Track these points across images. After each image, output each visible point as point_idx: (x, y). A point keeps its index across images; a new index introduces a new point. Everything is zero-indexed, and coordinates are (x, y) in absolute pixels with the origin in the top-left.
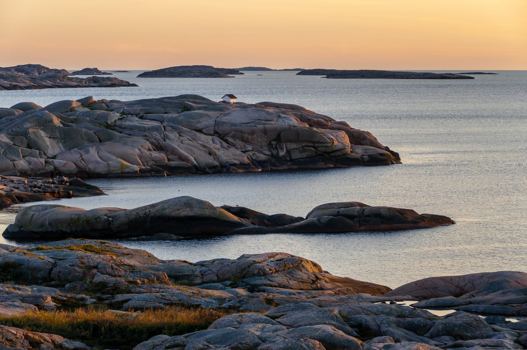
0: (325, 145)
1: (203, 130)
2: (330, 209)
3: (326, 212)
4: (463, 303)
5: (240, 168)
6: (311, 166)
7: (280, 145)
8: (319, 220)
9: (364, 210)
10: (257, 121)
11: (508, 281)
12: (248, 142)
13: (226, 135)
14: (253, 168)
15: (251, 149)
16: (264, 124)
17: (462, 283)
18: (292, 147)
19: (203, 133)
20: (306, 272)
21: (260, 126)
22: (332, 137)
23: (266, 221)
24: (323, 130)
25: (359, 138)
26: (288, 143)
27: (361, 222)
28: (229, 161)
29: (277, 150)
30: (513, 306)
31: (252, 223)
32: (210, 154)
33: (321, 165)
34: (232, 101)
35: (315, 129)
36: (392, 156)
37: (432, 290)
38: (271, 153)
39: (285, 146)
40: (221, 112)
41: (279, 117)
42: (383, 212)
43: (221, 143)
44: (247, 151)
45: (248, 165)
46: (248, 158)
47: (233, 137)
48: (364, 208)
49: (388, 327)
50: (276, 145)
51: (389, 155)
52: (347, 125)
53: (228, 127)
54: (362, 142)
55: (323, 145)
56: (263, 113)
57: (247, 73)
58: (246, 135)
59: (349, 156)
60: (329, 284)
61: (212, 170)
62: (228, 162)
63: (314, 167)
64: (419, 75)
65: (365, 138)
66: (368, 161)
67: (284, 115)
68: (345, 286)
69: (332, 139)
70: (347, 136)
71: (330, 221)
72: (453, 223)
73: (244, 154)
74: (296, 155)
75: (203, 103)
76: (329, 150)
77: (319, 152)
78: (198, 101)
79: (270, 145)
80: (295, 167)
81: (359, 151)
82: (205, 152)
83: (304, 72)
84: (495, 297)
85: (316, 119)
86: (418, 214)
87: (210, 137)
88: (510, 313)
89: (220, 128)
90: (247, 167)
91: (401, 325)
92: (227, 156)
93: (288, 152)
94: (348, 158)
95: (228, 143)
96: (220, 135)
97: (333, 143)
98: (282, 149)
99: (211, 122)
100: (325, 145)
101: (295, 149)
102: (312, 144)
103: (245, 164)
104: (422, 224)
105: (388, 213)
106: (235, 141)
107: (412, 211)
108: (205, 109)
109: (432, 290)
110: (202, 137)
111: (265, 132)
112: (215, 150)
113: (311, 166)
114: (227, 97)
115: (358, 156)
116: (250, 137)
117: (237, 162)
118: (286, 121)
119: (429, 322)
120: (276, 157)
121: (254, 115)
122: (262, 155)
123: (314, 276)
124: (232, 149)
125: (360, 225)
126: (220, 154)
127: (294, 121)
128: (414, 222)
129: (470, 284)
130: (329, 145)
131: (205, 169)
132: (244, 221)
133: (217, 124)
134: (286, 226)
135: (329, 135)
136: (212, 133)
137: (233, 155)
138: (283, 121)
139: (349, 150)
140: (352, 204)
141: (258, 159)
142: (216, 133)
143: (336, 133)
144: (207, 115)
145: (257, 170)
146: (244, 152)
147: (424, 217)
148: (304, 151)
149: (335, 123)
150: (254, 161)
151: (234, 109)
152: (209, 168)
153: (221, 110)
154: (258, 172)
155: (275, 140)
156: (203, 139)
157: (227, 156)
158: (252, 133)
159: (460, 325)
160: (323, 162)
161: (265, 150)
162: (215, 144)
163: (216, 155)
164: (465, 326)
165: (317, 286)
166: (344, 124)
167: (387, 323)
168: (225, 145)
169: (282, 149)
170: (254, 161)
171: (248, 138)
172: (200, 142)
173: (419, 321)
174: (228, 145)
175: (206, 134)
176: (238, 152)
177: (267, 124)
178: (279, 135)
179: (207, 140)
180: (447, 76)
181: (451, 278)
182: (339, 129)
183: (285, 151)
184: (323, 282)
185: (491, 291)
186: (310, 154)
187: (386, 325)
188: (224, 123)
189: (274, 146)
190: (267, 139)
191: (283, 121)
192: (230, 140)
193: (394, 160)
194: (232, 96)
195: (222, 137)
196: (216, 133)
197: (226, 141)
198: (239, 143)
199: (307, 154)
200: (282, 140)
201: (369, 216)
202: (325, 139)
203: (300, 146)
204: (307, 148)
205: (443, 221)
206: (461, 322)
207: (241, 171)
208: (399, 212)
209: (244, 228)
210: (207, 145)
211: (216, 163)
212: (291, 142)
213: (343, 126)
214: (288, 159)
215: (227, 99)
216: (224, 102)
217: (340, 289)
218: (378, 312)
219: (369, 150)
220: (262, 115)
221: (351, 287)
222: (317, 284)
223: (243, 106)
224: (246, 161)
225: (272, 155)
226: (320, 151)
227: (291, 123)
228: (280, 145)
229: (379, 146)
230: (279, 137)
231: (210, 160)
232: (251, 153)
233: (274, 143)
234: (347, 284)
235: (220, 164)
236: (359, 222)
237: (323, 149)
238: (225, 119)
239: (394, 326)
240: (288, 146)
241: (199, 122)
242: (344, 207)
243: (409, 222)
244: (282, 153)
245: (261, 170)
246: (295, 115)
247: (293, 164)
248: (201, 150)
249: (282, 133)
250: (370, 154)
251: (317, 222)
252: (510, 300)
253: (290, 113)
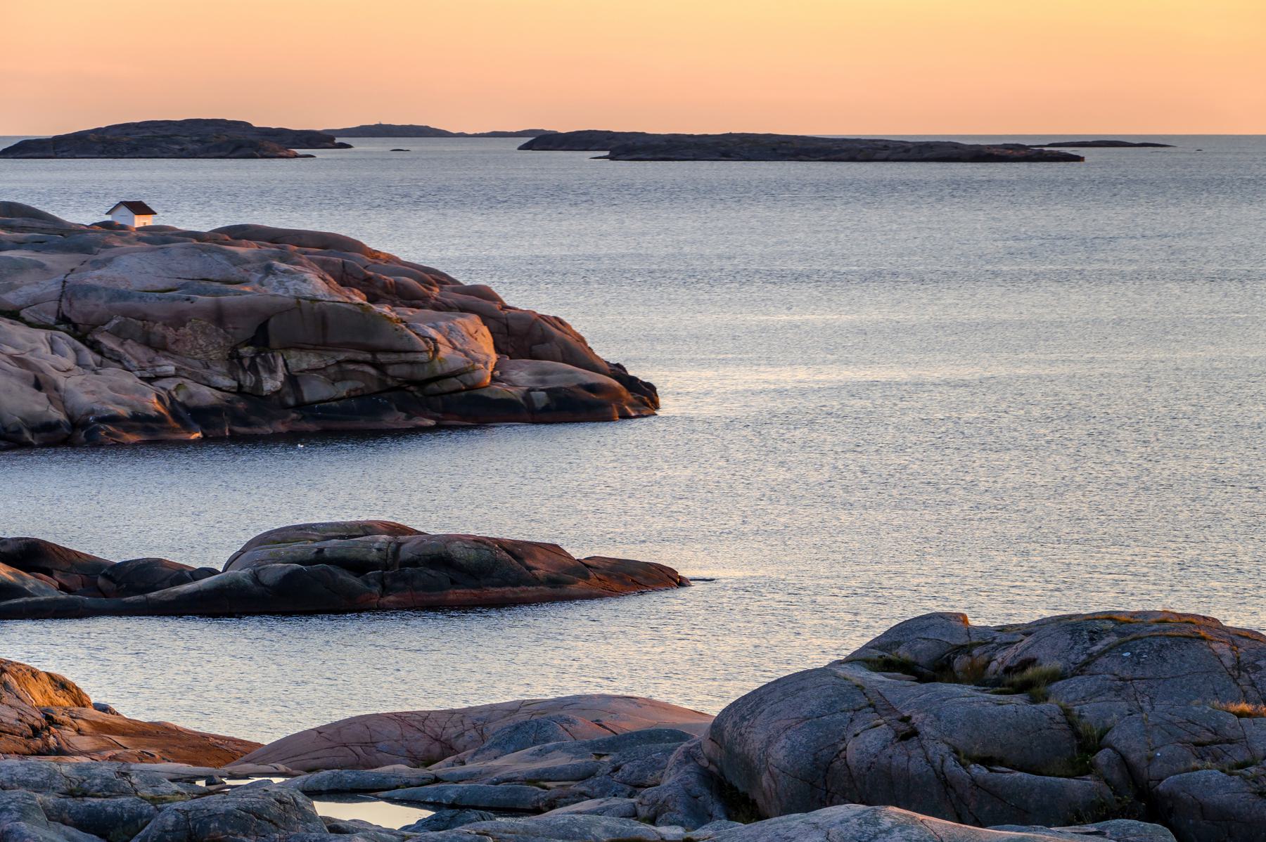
0: (411, 357)
1: (23, 313)
2: (297, 541)
3: (283, 550)
4: (414, 781)
5: (129, 430)
6: (362, 423)
7: (265, 360)
8: (256, 577)
9: (399, 545)
10: (196, 285)
11: (567, 720)
12: (165, 349)
13: (94, 326)
14: (174, 431)
15: (171, 369)
16: (217, 293)
17: (451, 730)
18: (305, 366)
19: (22, 320)
20: (15, 702)
21: (204, 300)
22: (432, 333)
23: (101, 581)
24: (408, 312)
25: (524, 336)
26: (292, 353)
27: (388, 581)
28: (97, 407)
29: (257, 373)
30: (544, 787)
31: (62, 587)
32: (38, 386)
33: (395, 419)
34: (140, 221)
35: (385, 310)
36: (624, 392)
37: (359, 750)
38: (235, 384)
39: (280, 362)
40: (83, 257)
41: (269, 270)
42: (458, 551)
43: (76, 351)
44: (158, 378)
45: (160, 419)
46: (159, 398)
47: (117, 333)
48: (401, 538)
49: (18, 820)
50: (253, 359)
51: (615, 388)
52: (492, 297)
53: (101, 302)
54: (537, 349)
55: (403, 357)
56: (217, 257)
57: (361, 146)
58: (158, 328)
59: (485, 393)
60: (87, 739)
61: (44, 434)
62: (92, 412)
63: (372, 425)
64: (907, 150)
65: (546, 338)
66: (546, 409)
67: (284, 266)
68: (137, 746)
69: (435, 341)
70: (485, 330)
71: (290, 577)
72: (682, 583)
73: (147, 387)
74: (316, 390)
75: (32, 229)
76: (423, 373)
77: (390, 382)
78: (18, 221)
79: (234, 360)
80: (311, 426)
81: (523, 376)
82: (24, 378)
83: (543, 141)
84: (516, 763)
85: (392, 279)
86: (569, 557)
87: (42, 334)
88: (529, 807)
89: (77, 304)
90: (154, 425)
91: (65, 815)
92: (93, 393)
93: (293, 380)
94: (487, 399)
95: (101, 353)
96: (75, 326)
97: (436, 351)
98: (272, 371)
99: (51, 287)
100: (411, 357)
101: (315, 370)
102: (369, 356)
103: (149, 418)
104: (580, 586)
105: (473, 553)
106: (122, 344)
107: (555, 549)
108: (38, 246)
109: (359, 750)
110: (19, 332)
111: (219, 316)
112: (55, 375)
113: (362, 423)
114: (124, 211)
115: (515, 393)
116: (170, 334)
117: (123, 411)
118: (290, 284)
119: (148, 807)
120: (253, 396)
121: (186, 265)
122: (206, 390)
123: (39, 716)
124: (113, 373)
125: (386, 590)
126: (71, 386)
127: (314, 284)
128: (553, 582)
129: (473, 732)
130: (423, 357)
131: (19, 431)
132: (30, 581)
133: (67, 292)
134: (152, 595)
135: (424, 327)
136: (52, 319)
137: (112, 389)
138: (281, 283)
139: (486, 375)
140: (367, 529)
141: (194, 402)
142: (63, 319)
143: (447, 319)
144: (41, 266)
145: (184, 436)
146: (149, 380)
147: (585, 568)
148: (343, 376)
149: (454, 290)
150: (181, 410)
151: (127, 246)
152: (34, 430)
153: (84, 249)
154: (189, 442)
155: (248, 343)
156: (20, 340)
157: (93, 393)
158: (178, 320)
159: (228, 813)
160: (400, 409)
161: (219, 374)
162: (56, 356)
163: (57, 389)
164: (241, 818)
165: (47, 744)
166: (483, 293)
167: (21, 810)
168: (90, 357)
169: (272, 371)
170: (181, 410)
171: (164, 337)
172: (10, 350)
173: (121, 806)
174: (98, 358)
175: (30, 325)
176: (130, 380)
177: (226, 293)
178: (263, 328)
179: (34, 343)
180: (995, 152)
181: (425, 717)
182: (464, 309)
183: (281, 375)
184: (68, 733)
185: (512, 748)
186: (361, 385)
187: (16, 815)
188: (90, 290)
189: (247, 362)
190: (225, 338)
191: (281, 283)
192: (108, 342)
193: (631, 405)
194: (140, 208)
195: (82, 332)
196: (63, 319)
197: (95, 346)
198: (135, 352)
199: (350, 385)
200: (274, 343)
201: (412, 563)
202: (410, 339)
203: (331, 362)
204: (351, 367)
205: (661, 578)
206: (231, 806)
207: (132, 438)
208: (508, 552)
209: (21, 600)
210: (32, 359)
211: (57, 415)
212: (301, 349)
213: (479, 301)
214: (291, 401)
215: (123, 217)
216: (106, 225)
217: (117, 752)
218: (12, 781)
219: (552, 373)
220: (216, 265)
221: (156, 746)
222: (45, 740)
223: (161, 237)
224: (152, 404)
225: (240, 390)
226: (393, 378)
227: (307, 290)
228: (265, 360)
229: (592, 364)
230: (262, 334)
231: (39, 405)
232: (170, 385)
233: (246, 351)
234: (146, 740)
235: (70, 417)
236: (381, 580)
237: (404, 370)
238: (93, 277)
239: (42, 817)
240: (292, 362)
241: (11, 287)
242: (342, 537)
243: (536, 581)
244: (271, 384)
245: (199, 435)
246: (324, 265)
247: (304, 418)
248: (11, 374)
249: (272, 320)
250: (555, 386)
251: (249, 582)
252: (546, 771)
253: (304, 259)
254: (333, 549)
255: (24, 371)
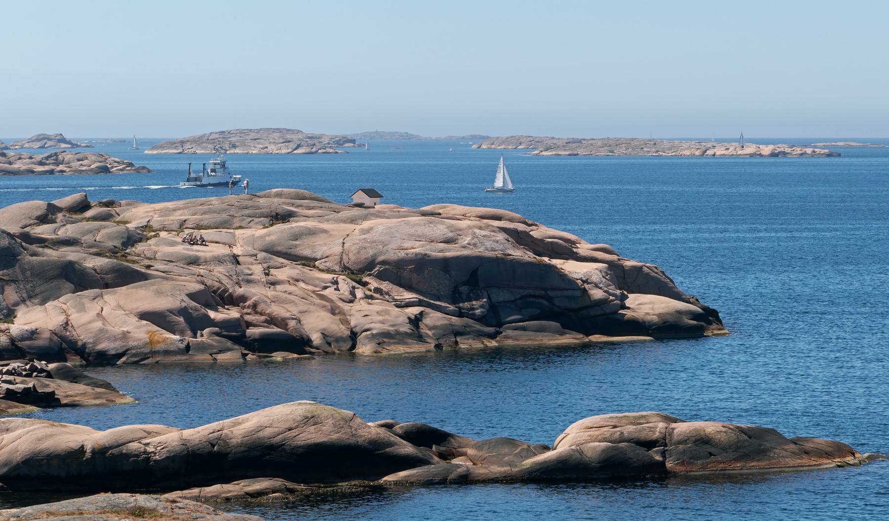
18: (501, 299)
32: (333, 312)
48: (674, 425)
100: (569, 293)
144: (325, 231)
155: (465, 283)
178: (474, 274)
204: (532, 299)
233: (464, 289)
254: (629, 433)
255: (325, 303)
